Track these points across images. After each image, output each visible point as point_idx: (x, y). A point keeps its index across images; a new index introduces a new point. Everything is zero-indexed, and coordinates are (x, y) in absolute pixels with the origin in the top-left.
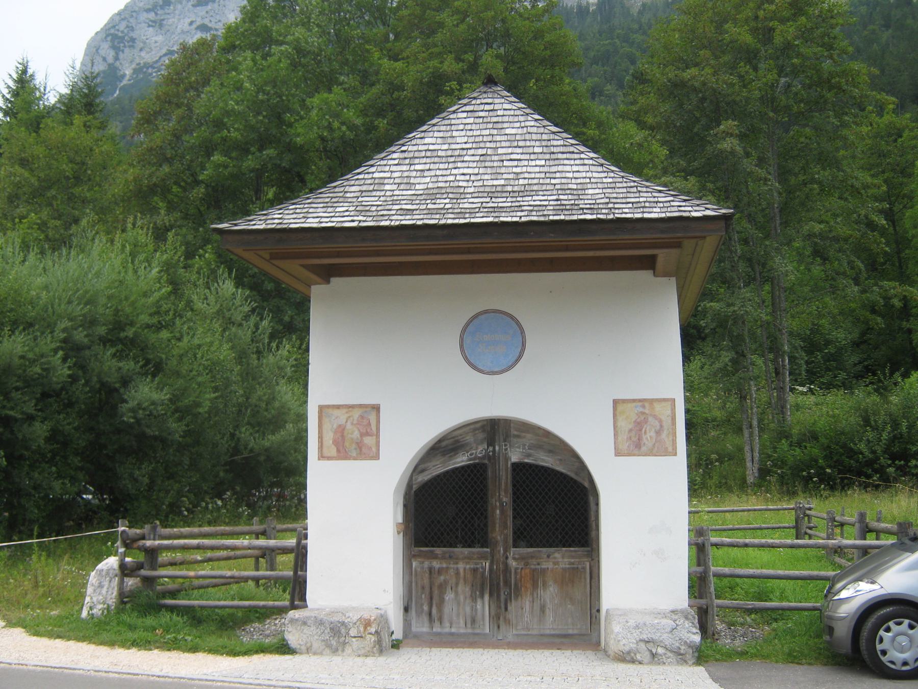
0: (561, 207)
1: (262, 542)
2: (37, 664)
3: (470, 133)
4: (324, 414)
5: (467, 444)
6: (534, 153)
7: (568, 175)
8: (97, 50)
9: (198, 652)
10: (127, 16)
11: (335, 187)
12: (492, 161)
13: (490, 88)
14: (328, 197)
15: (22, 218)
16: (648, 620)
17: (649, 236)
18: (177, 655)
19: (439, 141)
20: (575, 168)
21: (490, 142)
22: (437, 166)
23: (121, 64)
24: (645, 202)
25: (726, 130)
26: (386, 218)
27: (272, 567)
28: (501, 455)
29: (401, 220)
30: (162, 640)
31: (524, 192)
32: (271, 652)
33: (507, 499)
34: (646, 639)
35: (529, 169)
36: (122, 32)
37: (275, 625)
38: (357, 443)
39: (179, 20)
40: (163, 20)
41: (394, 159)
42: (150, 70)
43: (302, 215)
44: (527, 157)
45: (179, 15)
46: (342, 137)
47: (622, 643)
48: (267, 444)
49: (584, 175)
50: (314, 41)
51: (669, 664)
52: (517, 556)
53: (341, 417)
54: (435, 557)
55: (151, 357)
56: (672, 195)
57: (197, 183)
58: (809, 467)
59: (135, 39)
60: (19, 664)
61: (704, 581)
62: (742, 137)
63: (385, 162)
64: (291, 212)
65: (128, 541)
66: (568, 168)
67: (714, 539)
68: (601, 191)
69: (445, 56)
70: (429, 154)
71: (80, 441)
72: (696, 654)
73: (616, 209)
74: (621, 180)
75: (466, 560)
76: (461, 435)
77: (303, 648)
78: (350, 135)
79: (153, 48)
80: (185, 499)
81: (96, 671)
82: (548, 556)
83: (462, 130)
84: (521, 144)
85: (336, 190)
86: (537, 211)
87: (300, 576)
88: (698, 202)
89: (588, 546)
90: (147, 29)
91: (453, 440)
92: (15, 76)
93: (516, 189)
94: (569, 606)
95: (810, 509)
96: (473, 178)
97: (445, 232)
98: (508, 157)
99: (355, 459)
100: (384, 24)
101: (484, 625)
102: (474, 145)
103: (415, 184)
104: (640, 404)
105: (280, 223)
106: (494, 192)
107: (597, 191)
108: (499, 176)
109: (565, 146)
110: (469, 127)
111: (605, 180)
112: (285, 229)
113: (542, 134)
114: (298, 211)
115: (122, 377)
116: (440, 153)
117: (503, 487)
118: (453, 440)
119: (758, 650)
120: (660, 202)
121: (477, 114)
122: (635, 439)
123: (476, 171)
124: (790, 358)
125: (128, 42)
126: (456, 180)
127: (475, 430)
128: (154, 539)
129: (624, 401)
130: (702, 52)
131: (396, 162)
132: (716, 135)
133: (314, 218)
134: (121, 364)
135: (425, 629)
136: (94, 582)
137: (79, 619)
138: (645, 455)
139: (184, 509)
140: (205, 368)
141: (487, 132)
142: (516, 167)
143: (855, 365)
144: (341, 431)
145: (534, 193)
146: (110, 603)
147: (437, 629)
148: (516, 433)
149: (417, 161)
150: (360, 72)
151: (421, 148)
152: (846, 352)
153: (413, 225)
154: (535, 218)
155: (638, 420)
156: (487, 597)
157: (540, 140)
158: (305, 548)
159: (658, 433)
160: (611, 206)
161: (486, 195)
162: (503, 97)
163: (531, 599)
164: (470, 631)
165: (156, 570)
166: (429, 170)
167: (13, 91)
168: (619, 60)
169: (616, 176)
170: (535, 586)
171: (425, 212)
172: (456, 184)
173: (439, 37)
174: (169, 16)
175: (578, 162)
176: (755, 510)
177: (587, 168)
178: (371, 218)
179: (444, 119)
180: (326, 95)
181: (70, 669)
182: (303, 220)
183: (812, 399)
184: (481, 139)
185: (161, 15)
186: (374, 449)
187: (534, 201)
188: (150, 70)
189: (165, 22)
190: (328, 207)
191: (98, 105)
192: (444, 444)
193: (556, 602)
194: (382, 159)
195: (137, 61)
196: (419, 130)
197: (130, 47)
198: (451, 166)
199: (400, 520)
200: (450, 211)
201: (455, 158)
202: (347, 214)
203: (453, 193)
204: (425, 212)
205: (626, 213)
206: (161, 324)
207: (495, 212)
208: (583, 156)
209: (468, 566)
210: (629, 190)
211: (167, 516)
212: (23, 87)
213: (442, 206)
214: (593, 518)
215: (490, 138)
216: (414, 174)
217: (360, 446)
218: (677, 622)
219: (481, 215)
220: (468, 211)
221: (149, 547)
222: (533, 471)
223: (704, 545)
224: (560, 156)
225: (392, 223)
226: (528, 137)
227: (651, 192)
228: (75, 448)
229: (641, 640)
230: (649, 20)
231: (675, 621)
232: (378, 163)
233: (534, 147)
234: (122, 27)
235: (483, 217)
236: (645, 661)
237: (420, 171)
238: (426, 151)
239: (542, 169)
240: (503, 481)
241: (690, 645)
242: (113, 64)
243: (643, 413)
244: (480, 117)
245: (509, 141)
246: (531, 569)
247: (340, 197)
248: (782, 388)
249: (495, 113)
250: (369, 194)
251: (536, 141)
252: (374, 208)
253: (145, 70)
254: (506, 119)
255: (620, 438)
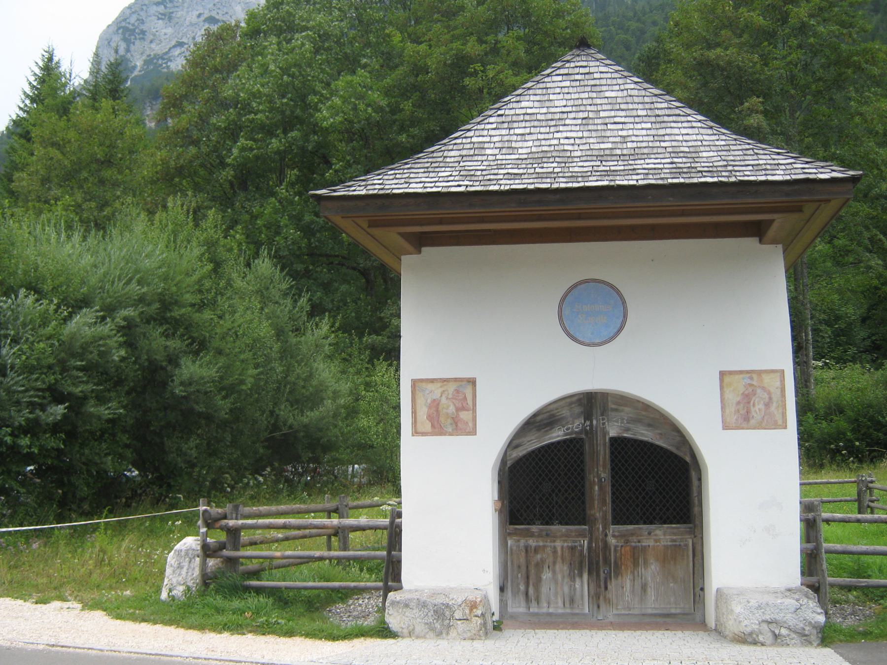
0: (678, 170)
1: (335, 521)
2: (130, 650)
3: (568, 97)
4: (417, 388)
5: (563, 418)
6: (639, 116)
7: (677, 138)
8: (109, 43)
9: (294, 636)
10: (138, 10)
11: (433, 152)
12: (594, 124)
13: (583, 51)
14: (428, 162)
15: (57, 199)
16: (771, 599)
17: (771, 200)
18: (273, 639)
19: (537, 104)
20: (684, 131)
21: (591, 105)
22: (538, 130)
23: (132, 56)
24: (765, 164)
25: (751, 107)
26: (495, 182)
27: (345, 547)
28: (599, 429)
29: (511, 185)
30: (254, 624)
31: (635, 155)
32: (372, 636)
33: (605, 474)
34: (769, 620)
35: (636, 132)
36: (133, 25)
37: (360, 605)
38: (453, 418)
39: (188, 12)
40: (172, 13)
41: (492, 123)
42: (160, 62)
43: (403, 181)
44: (631, 120)
45: (188, 8)
46: (367, 119)
47: (743, 624)
48: (305, 420)
49: (694, 137)
50: (336, 26)
51: (793, 645)
52: (616, 534)
53: (436, 391)
54: (532, 535)
55: (195, 335)
56: (792, 158)
57: (223, 164)
58: (837, 439)
59: (146, 31)
60: (111, 651)
61: (815, 557)
62: (765, 113)
63: (482, 126)
64: (391, 177)
65: (209, 521)
66: (676, 131)
67: (825, 515)
68: (715, 154)
69: (468, 38)
70: (527, 118)
71: (128, 419)
72: (820, 635)
73: (736, 171)
74: (734, 142)
75: (563, 539)
76: (557, 409)
77: (406, 631)
78: (376, 117)
79: (163, 40)
80: (227, 475)
81: (194, 658)
82: (649, 534)
83: (559, 93)
84: (623, 106)
85: (435, 155)
86: (652, 174)
87: (393, 556)
88: (822, 164)
89: (690, 523)
90: (156, 21)
91: (548, 414)
92: (41, 64)
93: (625, 152)
94: (672, 585)
95: (872, 482)
96: (578, 141)
97: (558, 196)
98: (612, 120)
99: (451, 435)
100: (404, 9)
101: (583, 605)
102: (574, 109)
103: (517, 148)
104: (748, 375)
105: (382, 189)
106: (602, 156)
107: (711, 154)
108: (606, 140)
109: (670, 108)
110: (566, 90)
111: (717, 143)
112: (388, 194)
113: (644, 96)
114: (398, 176)
115: (168, 356)
116: (539, 117)
117: (601, 463)
118: (548, 414)
119: (881, 630)
120: (781, 164)
121: (572, 77)
122: (743, 412)
123: (580, 134)
124: (813, 330)
125: (139, 34)
126: (560, 144)
127: (571, 404)
128: (237, 519)
129: (731, 373)
130: (723, 32)
131: (494, 126)
132: (740, 112)
133: (417, 183)
134: (168, 343)
135: (522, 609)
136: (173, 562)
137: (159, 601)
138: (754, 428)
139: (226, 485)
140: (247, 345)
141: (586, 95)
142: (621, 130)
143: (864, 339)
144: (435, 405)
145: (646, 156)
146: (190, 584)
147: (534, 609)
148: (613, 406)
149: (515, 125)
150: (383, 54)
151: (518, 111)
152: (855, 327)
153: (524, 189)
154: (653, 182)
155: (746, 392)
156: (585, 576)
157: (642, 103)
158: (399, 527)
159: (767, 405)
160: (730, 168)
161: (595, 158)
162: (598, 60)
163: (632, 578)
164: (568, 611)
165: (239, 550)
166: (530, 134)
167: (40, 78)
168: (615, 47)
169: (728, 138)
170: (636, 564)
171: (534, 176)
172: (561, 148)
173: (460, 19)
174: (177, 9)
175: (685, 125)
176: (816, 483)
177: (696, 131)
178: (478, 183)
179: (538, 82)
180: (349, 78)
181: (167, 656)
182: (406, 186)
183: (832, 373)
184: (580, 102)
185: (170, 8)
186: (470, 424)
187: (648, 164)
188: (160, 62)
189: (174, 15)
190: (430, 172)
191: (122, 91)
192: (539, 418)
193: (658, 580)
194: (479, 123)
195: (148, 53)
196: (514, 93)
197: (140, 39)
198: (552, 129)
199: (496, 498)
200: (560, 175)
201: (556, 122)
202: (451, 178)
203: (559, 157)
204: (534, 176)
205: (748, 176)
206: (204, 302)
207: (609, 176)
208: (689, 118)
209: (566, 544)
210: (745, 152)
211: (209, 493)
212: (49, 75)
213: (551, 170)
214: (695, 494)
215: (589, 101)
216: (515, 138)
217: (455, 421)
218: (801, 602)
219: (595, 178)
220: (579, 175)
221: (232, 527)
222: (632, 446)
223: (815, 520)
224: (666, 119)
225: (502, 188)
226: (629, 100)
227: (769, 155)
228: (123, 426)
229: (763, 621)
230: (643, 7)
231: (798, 600)
232: (475, 128)
233: (637, 109)
234: (133, 20)
235: (597, 181)
236: (768, 642)
237: (520, 135)
238: (524, 114)
239: (649, 132)
240: (601, 458)
241: (815, 626)
242: (124, 56)
243: (751, 385)
244: (577, 80)
245: (610, 104)
246: (631, 546)
247: (440, 162)
248: (805, 362)
249: (591, 76)
250: (470, 158)
251: (638, 103)
252: (479, 173)
253: (155, 61)
254: (604, 82)
255: (727, 411)
